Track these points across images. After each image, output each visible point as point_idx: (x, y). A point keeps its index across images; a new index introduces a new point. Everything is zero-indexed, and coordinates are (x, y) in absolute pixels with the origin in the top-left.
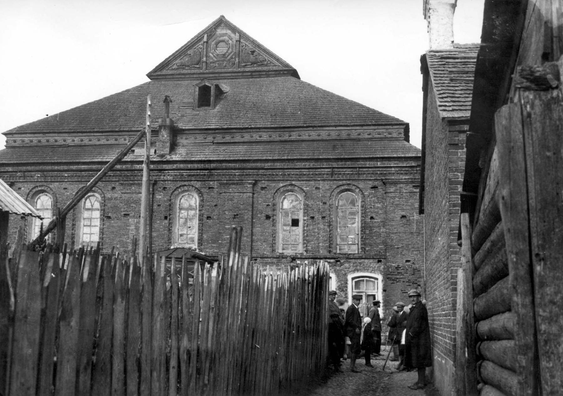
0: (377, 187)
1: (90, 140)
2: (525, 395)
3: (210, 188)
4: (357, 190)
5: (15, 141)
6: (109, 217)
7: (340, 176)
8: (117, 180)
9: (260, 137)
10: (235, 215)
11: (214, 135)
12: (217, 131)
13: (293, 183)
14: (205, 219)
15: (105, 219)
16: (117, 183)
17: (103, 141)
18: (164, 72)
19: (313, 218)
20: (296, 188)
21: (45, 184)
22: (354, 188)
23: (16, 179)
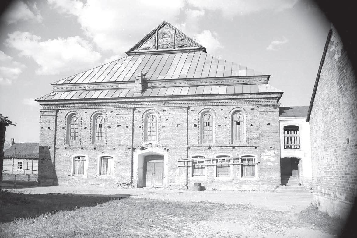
0: (254, 109)
1: (108, 87)
2: (13, 237)
3: (164, 111)
4: (244, 110)
5: (76, 88)
6: (110, 127)
7: (252, 103)
8: (114, 107)
9: (76, 88)
10: (178, 125)
11: (166, 83)
12: (167, 81)
13: (209, 107)
14: (161, 127)
15: (108, 128)
16: (114, 109)
17: (105, 87)
18: (135, 51)
19: (220, 126)
20: (210, 110)
21: (75, 110)
22: (242, 109)
23: (59, 108)
